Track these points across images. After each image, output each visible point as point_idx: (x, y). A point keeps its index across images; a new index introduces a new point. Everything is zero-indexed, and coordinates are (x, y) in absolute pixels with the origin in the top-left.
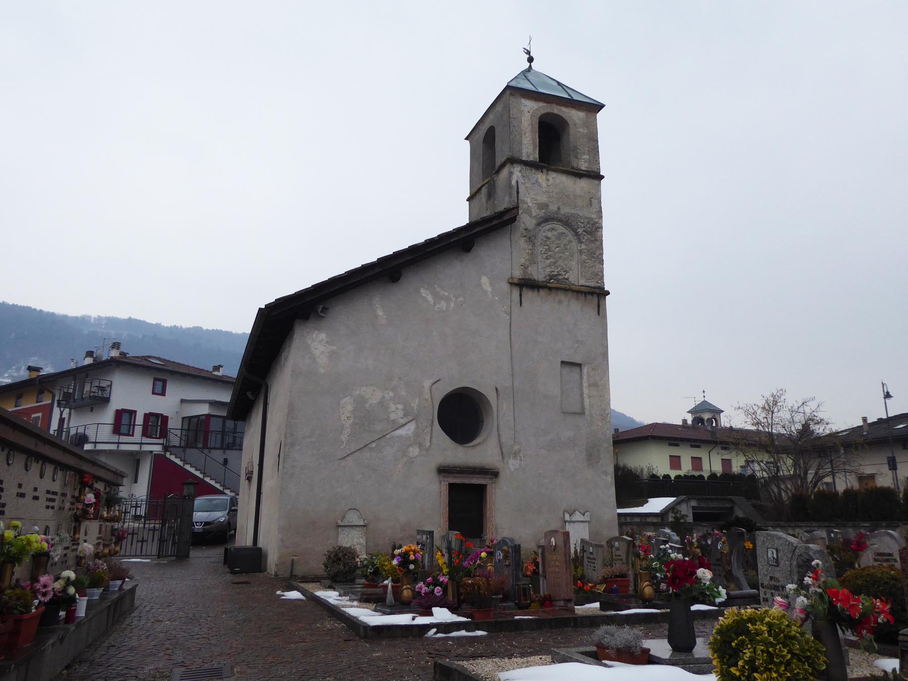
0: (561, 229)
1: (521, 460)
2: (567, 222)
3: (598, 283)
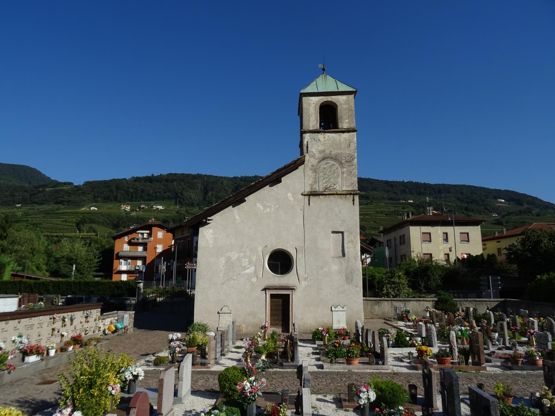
0: (332, 162)
2: (335, 158)
3: (353, 188)
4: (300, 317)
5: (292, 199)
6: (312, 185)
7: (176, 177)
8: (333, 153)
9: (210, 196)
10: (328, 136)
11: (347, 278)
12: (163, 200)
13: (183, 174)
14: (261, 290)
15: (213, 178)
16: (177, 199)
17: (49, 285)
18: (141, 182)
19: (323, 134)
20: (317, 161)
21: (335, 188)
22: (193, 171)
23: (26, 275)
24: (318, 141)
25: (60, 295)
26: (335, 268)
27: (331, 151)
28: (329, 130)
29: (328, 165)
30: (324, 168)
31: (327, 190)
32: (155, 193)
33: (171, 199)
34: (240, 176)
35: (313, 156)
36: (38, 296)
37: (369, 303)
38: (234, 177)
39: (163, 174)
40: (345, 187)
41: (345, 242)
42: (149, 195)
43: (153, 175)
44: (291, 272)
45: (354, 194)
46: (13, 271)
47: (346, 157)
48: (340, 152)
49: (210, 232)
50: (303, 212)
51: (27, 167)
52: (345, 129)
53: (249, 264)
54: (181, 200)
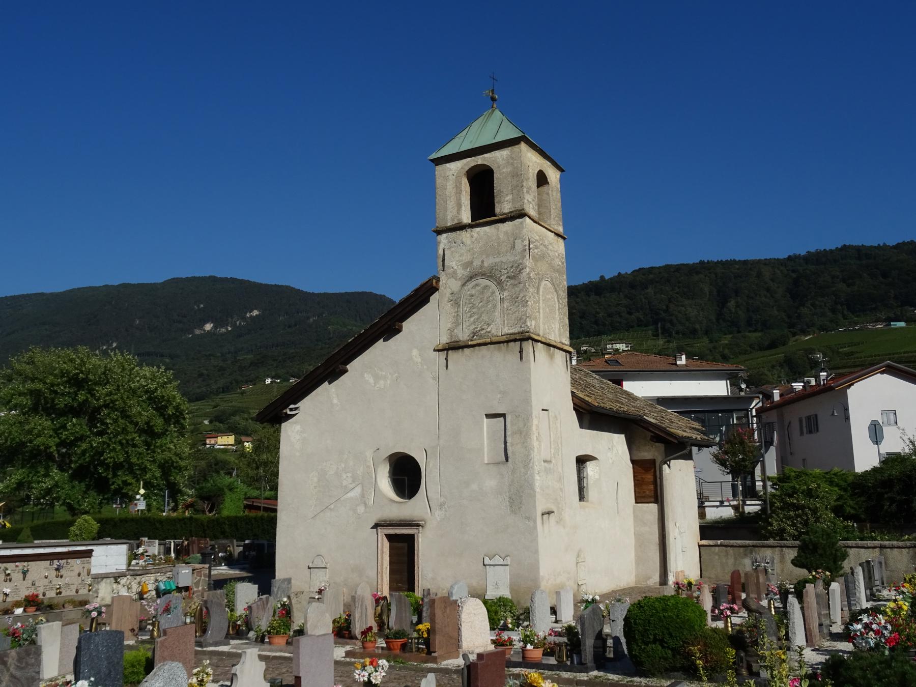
0: (484, 282)
1: (446, 511)
2: (489, 274)
3: (521, 327)
4: (430, 575)
5: (420, 360)
6: (451, 330)
7: (651, 276)
8: (486, 264)
9: (733, 310)
10: (478, 233)
11: (512, 503)
12: (627, 330)
13: (667, 267)
14: (372, 528)
15: (737, 267)
16: (657, 324)
17: (224, 523)
18: (577, 297)
19: (469, 230)
20: (460, 283)
21: (489, 332)
22: (690, 257)
23: (262, 505)
24: (461, 245)
25: (235, 540)
26: (490, 483)
27: (483, 262)
28: (478, 222)
29: (478, 288)
30: (472, 296)
31: (475, 337)
32: (610, 315)
33: (646, 326)
34: (803, 253)
35: (454, 275)
36: (209, 542)
37: (731, 551)
38: (790, 256)
39: (623, 272)
40: (506, 328)
41: (508, 433)
42: (596, 323)
43: (602, 277)
44: (417, 495)
45: (522, 340)
46: (246, 499)
47: (509, 269)
48: (498, 260)
49: (296, 430)
50: (436, 382)
51: (370, 295)
52: (505, 214)
53: (354, 481)
54: (668, 325)
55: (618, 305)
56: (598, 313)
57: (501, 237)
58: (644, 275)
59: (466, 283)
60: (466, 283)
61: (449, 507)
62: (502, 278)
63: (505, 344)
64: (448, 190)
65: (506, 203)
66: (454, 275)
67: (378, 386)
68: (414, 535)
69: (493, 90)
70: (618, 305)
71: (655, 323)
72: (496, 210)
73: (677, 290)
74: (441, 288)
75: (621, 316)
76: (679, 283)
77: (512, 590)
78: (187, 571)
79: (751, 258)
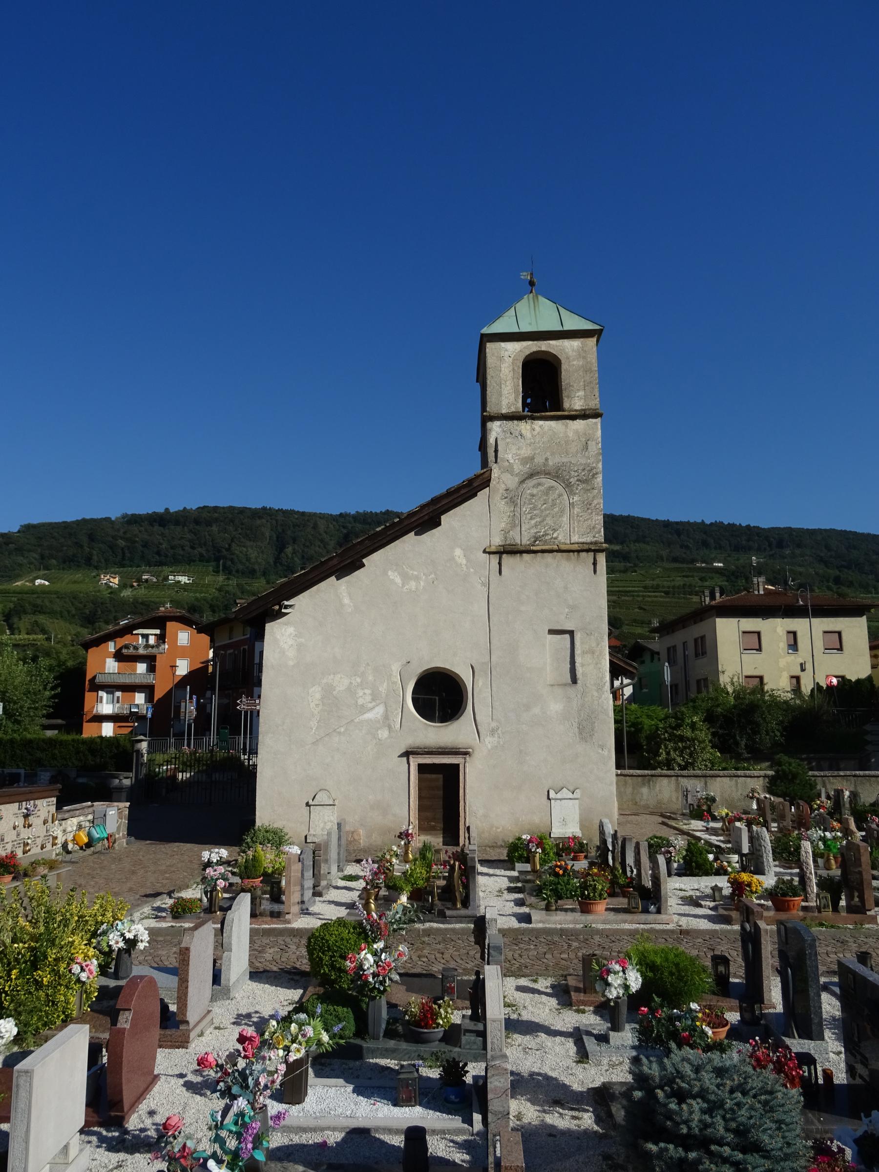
0: (549, 482)
1: (499, 737)
2: (556, 474)
3: (594, 537)
4: (481, 812)
5: (464, 562)
6: (506, 532)
8: (550, 463)
9: (290, 555)
10: (541, 427)
11: (581, 730)
12: (189, 564)
13: (231, 508)
14: (399, 757)
15: (296, 516)
16: (219, 561)
19: (529, 421)
20: (517, 479)
21: (556, 538)
24: (520, 437)
26: (555, 707)
27: (547, 459)
28: (543, 414)
29: (540, 488)
30: (533, 495)
33: (208, 561)
35: (509, 470)
37: (630, 781)
39: (188, 508)
41: (578, 652)
43: (167, 509)
44: (462, 718)
48: (565, 460)
50: (486, 589)
52: (576, 411)
53: (373, 700)
54: (229, 563)
55: (182, 538)
56: (161, 544)
57: (571, 435)
58: (209, 512)
59: (525, 480)
60: (525, 480)
61: (503, 733)
62: (571, 480)
63: (576, 553)
64: (503, 372)
65: (576, 398)
66: (509, 470)
67: (407, 587)
68: (458, 765)
69: (532, 274)
70: (182, 538)
71: (217, 560)
72: (564, 404)
73: (240, 531)
74: (493, 483)
75: (183, 550)
76: (242, 524)
77: (582, 827)
78: (113, 812)
79: (310, 511)
